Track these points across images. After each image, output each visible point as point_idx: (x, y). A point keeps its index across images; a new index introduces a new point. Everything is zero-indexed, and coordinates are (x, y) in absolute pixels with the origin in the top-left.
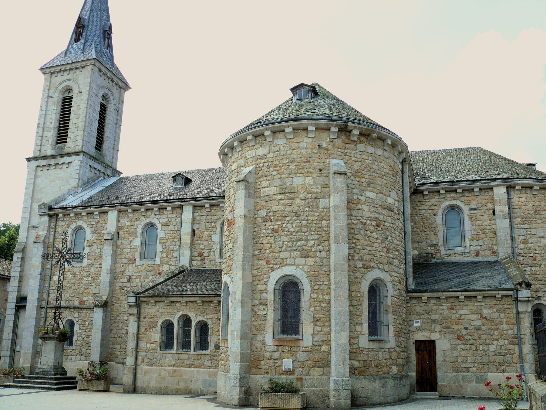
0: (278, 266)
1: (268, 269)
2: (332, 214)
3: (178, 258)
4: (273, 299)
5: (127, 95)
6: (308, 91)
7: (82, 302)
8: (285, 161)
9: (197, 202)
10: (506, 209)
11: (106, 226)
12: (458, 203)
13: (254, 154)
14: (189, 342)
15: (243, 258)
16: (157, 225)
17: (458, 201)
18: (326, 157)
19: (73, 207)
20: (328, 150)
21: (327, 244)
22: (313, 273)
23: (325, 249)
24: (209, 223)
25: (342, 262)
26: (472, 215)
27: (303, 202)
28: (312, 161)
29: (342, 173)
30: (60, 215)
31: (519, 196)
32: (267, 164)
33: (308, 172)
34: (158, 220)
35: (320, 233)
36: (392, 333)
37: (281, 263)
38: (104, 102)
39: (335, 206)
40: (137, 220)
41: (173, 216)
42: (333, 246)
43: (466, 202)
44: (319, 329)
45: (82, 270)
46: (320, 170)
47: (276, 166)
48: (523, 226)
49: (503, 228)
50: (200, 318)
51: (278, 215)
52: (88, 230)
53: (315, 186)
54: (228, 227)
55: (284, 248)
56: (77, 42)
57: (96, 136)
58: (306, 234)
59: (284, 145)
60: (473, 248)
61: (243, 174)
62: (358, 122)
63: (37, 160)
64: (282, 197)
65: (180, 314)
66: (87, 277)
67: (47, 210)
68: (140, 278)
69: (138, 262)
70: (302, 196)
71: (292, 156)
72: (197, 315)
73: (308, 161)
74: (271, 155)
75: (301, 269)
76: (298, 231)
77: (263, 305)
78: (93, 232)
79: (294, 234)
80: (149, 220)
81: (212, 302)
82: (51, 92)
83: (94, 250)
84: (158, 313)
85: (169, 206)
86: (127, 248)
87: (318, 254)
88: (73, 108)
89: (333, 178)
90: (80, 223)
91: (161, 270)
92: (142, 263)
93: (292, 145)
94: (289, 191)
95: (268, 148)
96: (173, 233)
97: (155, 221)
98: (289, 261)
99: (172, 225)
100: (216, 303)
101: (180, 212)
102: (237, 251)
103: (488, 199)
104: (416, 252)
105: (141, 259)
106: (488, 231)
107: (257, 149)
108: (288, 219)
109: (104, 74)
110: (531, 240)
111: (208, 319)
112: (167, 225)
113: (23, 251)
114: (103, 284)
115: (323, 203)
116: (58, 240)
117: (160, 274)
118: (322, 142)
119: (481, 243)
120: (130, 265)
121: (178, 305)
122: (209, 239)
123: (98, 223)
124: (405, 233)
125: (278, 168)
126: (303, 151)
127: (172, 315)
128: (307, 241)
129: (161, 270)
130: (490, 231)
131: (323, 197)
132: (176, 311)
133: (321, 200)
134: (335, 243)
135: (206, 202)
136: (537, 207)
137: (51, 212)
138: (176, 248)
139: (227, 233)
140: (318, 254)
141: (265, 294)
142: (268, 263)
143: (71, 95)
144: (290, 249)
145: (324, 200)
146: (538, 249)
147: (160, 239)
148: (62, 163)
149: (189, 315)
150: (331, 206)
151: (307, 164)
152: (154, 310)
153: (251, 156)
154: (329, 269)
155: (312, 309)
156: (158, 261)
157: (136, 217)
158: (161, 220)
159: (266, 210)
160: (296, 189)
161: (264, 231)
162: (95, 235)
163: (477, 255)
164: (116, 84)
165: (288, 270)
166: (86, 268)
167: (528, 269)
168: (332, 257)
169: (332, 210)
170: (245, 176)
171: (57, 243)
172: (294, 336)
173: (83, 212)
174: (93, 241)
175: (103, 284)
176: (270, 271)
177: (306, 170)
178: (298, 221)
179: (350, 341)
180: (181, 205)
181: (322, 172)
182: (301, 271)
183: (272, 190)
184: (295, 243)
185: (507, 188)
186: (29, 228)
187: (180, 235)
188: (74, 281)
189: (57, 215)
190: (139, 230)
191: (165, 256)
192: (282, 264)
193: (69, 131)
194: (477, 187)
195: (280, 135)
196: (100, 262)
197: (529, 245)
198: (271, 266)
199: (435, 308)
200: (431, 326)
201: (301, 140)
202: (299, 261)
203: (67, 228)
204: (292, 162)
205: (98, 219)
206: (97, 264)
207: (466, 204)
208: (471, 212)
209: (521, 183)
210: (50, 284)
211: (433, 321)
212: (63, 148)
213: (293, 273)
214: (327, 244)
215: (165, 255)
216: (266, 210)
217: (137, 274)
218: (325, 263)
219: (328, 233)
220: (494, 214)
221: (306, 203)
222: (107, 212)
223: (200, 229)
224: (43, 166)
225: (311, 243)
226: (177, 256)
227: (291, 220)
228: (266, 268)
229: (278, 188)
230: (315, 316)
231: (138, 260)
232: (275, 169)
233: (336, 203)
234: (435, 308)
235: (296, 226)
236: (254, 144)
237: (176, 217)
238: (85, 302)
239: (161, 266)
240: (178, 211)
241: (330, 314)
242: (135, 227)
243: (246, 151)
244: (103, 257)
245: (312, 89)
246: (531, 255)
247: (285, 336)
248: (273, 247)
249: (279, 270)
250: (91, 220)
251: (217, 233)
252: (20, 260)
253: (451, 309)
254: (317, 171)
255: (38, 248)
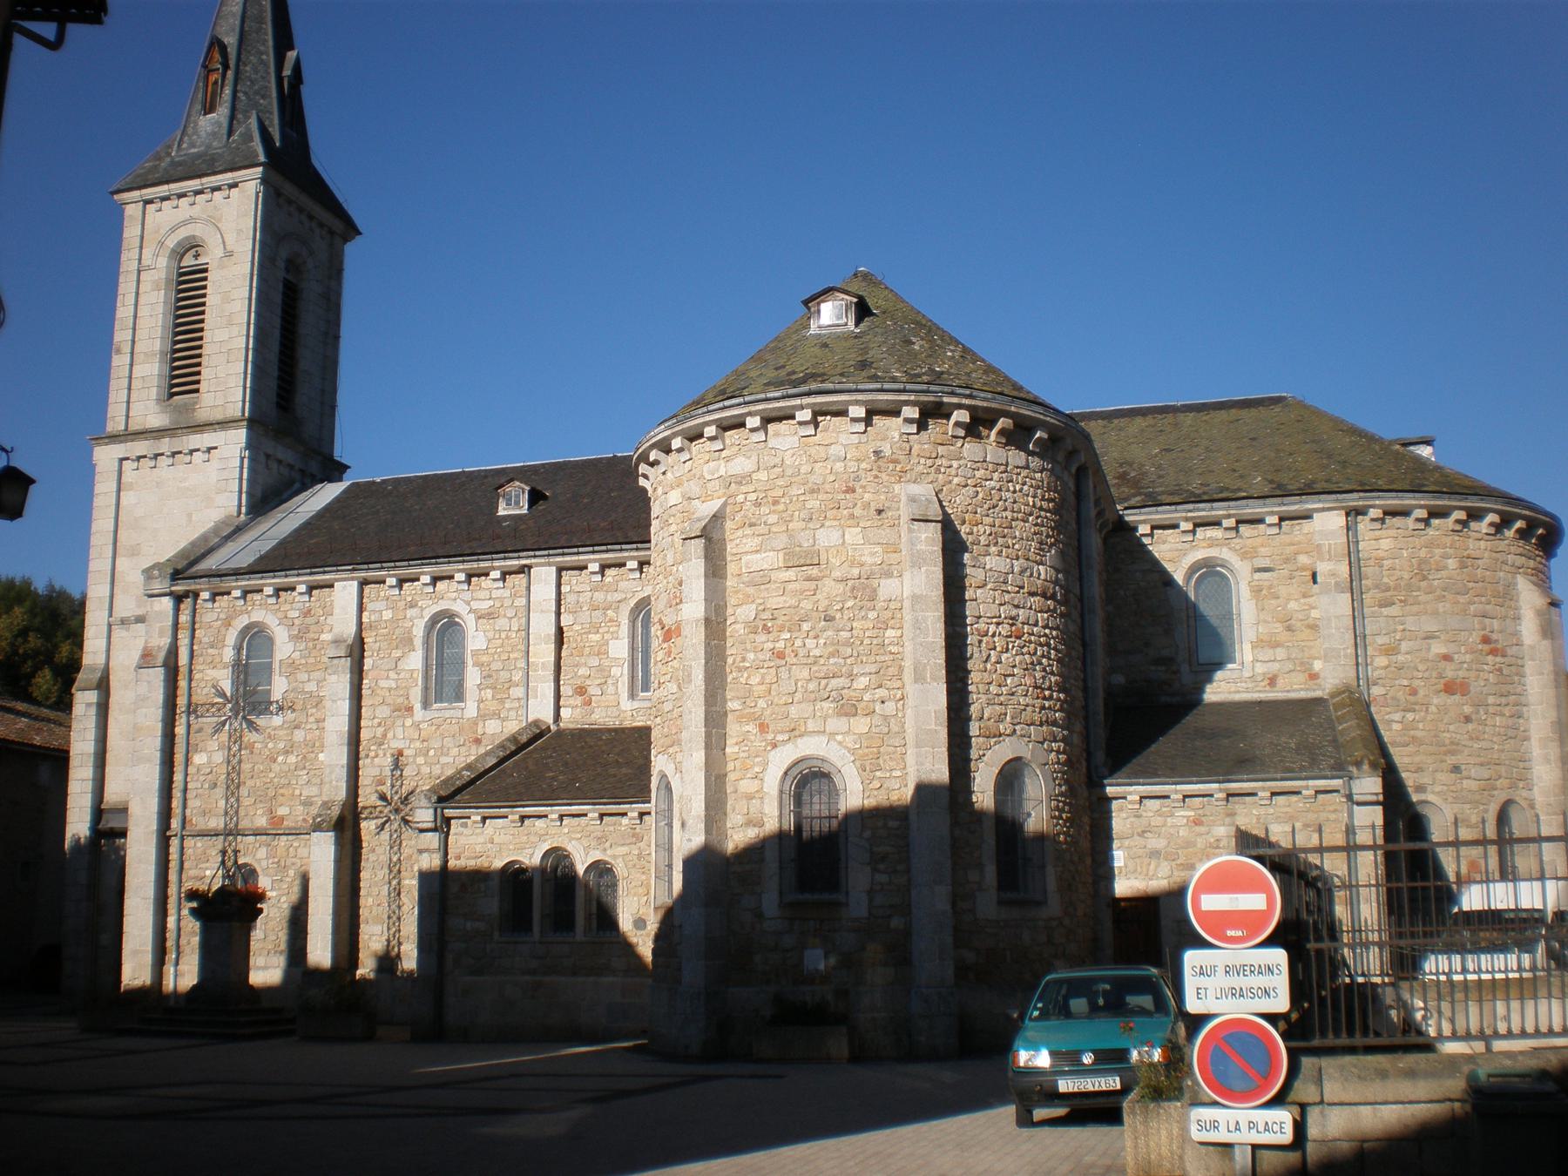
0: (786, 737)
1: (764, 744)
2: (908, 617)
3: (523, 702)
4: (776, 813)
5: (353, 252)
6: (847, 305)
7: (276, 821)
8: (795, 491)
9: (568, 558)
10: (1343, 569)
11: (328, 621)
12: (1224, 554)
13: (722, 472)
14: (572, 914)
15: (706, 720)
16: (465, 617)
17: (1225, 550)
18: (893, 479)
19: (237, 573)
20: (896, 462)
21: (899, 684)
22: (866, 751)
23: (895, 696)
24: (601, 612)
25: (933, 727)
26: (1261, 583)
27: (841, 586)
28: (859, 490)
29: (930, 518)
30: (205, 595)
31: (1377, 533)
32: (753, 497)
33: (852, 516)
34: (468, 603)
35: (882, 658)
36: (1052, 883)
37: (793, 730)
38: (290, 278)
39: (915, 598)
40: (412, 605)
41: (507, 593)
42: (911, 688)
43: (1246, 553)
44: (883, 878)
45: (270, 737)
46: (880, 512)
47: (775, 503)
48: (1385, 611)
49: (1336, 617)
50: (596, 855)
51: (783, 618)
52: (281, 635)
53: (867, 549)
54: (665, 641)
55: (798, 696)
56: (210, 112)
57: (276, 374)
58: (849, 661)
59: (791, 451)
60: (1260, 668)
61: (699, 520)
62: (968, 392)
63: (121, 442)
64: (791, 574)
65: (546, 847)
66: (287, 753)
67: (167, 583)
68: (426, 755)
69: (419, 713)
70: (837, 574)
71: (812, 478)
72: (587, 849)
73: (852, 490)
74: (763, 476)
75: (840, 743)
76: (832, 655)
77: (755, 826)
78: (296, 638)
79: (822, 661)
80: (442, 605)
81: (625, 814)
82: (147, 253)
83: (301, 685)
84: (490, 846)
85: (494, 568)
86: (388, 678)
87: (878, 707)
88: (212, 299)
89: (910, 531)
90: (258, 616)
91: (480, 731)
92: (429, 715)
93: (813, 451)
94: (808, 562)
95: (754, 458)
96: (507, 637)
97: (459, 607)
98: (811, 726)
99: (505, 616)
100: (634, 819)
101: (525, 581)
102: (689, 703)
103: (1299, 543)
104: (1119, 679)
105: (426, 705)
106: (1299, 624)
107: (728, 459)
108: (806, 626)
109: (290, 202)
110: (1404, 646)
111: (615, 857)
112: (490, 616)
113: (103, 686)
114: (331, 773)
115: (887, 588)
116: (201, 659)
117: (478, 741)
118: (883, 443)
119: (1281, 653)
120: (399, 722)
121: (539, 823)
122: (601, 651)
123: (307, 613)
124: (1084, 645)
125: (781, 507)
126: (839, 466)
127: (527, 851)
128: (851, 676)
129: (480, 731)
130: (1306, 622)
131: (889, 575)
132: (533, 839)
133: (883, 582)
134: (916, 681)
135: (592, 557)
136: (1422, 562)
137: (180, 588)
138: (518, 676)
139: (660, 655)
140: (878, 707)
141: (759, 801)
142: (763, 728)
143: (201, 260)
144: (813, 696)
145: (889, 581)
146: (1421, 667)
147: (475, 653)
148: (192, 452)
149: (568, 849)
150: (905, 596)
151: (848, 496)
152: (481, 839)
153: (716, 476)
154: (903, 742)
155: (867, 834)
156: (470, 709)
157: (409, 599)
158: (475, 605)
159: (754, 606)
160: (823, 557)
161: (751, 656)
162: (303, 646)
163: (1272, 681)
164: (321, 225)
165: (810, 746)
166: (281, 733)
167: (1397, 717)
168: (909, 712)
169: (907, 604)
170: (705, 527)
171: (198, 668)
172: (826, 896)
173: (265, 585)
174: (298, 662)
175: (331, 773)
176: (769, 748)
177: (845, 512)
178: (830, 633)
179: (954, 904)
180: (525, 566)
181: (883, 515)
182: (839, 748)
183: (769, 560)
184: (824, 682)
185: (1347, 515)
186: (110, 626)
187: (525, 642)
188: (251, 765)
189: (196, 595)
190: (419, 632)
191: (490, 696)
192: (795, 733)
193: (204, 360)
194: (1272, 513)
195: (783, 427)
196: (319, 715)
197: (1400, 658)
198: (770, 736)
199: (1158, 821)
200: (1149, 864)
201: (833, 440)
202: (836, 724)
203: (223, 629)
204: (812, 491)
205: (307, 605)
206: (311, 719)
207: (1245, 555)
208: (1257, 576)
209: (1382, 502)
210: (186, 775)
211: (1155, 854)
212: (189, 409)
213: (821, 753)
214: (899, 684)
215: (489, 693)
216: (754, 606)
217: (418, 744)
218: (895, 728)
219: (897, 658)
220: (1315, 582)
221: (848, 588)
222: (332, 586)
223: (577, 627)
224: (139, 458)
225: (862, 682)
226: (521, 696)
227: (813, 628)
228: (759, 744)
229: (781, 555)
230: (875, 849)
231: (418, 706)
232: (773, 508)
233: (917, 591)
234: (1158, 821)
235: (825, 644)
236: (722, 447)
237: (514, 596)
238: (282, 819)
239: (481, 725)
240: (519, 580)
241: (908, 845)
242: (408, 624)
243: (702, 461)
244: (328, 704)
245: (855, 300)
246: (1405, 682)
247: (807, 896)
248: (773, 693)
249: (789, 746)
250: (287, 607)
251: (621, 636)
252: (93, 711)
253: (1196, 824)
254: (872, 512)
255: (149, 682)
